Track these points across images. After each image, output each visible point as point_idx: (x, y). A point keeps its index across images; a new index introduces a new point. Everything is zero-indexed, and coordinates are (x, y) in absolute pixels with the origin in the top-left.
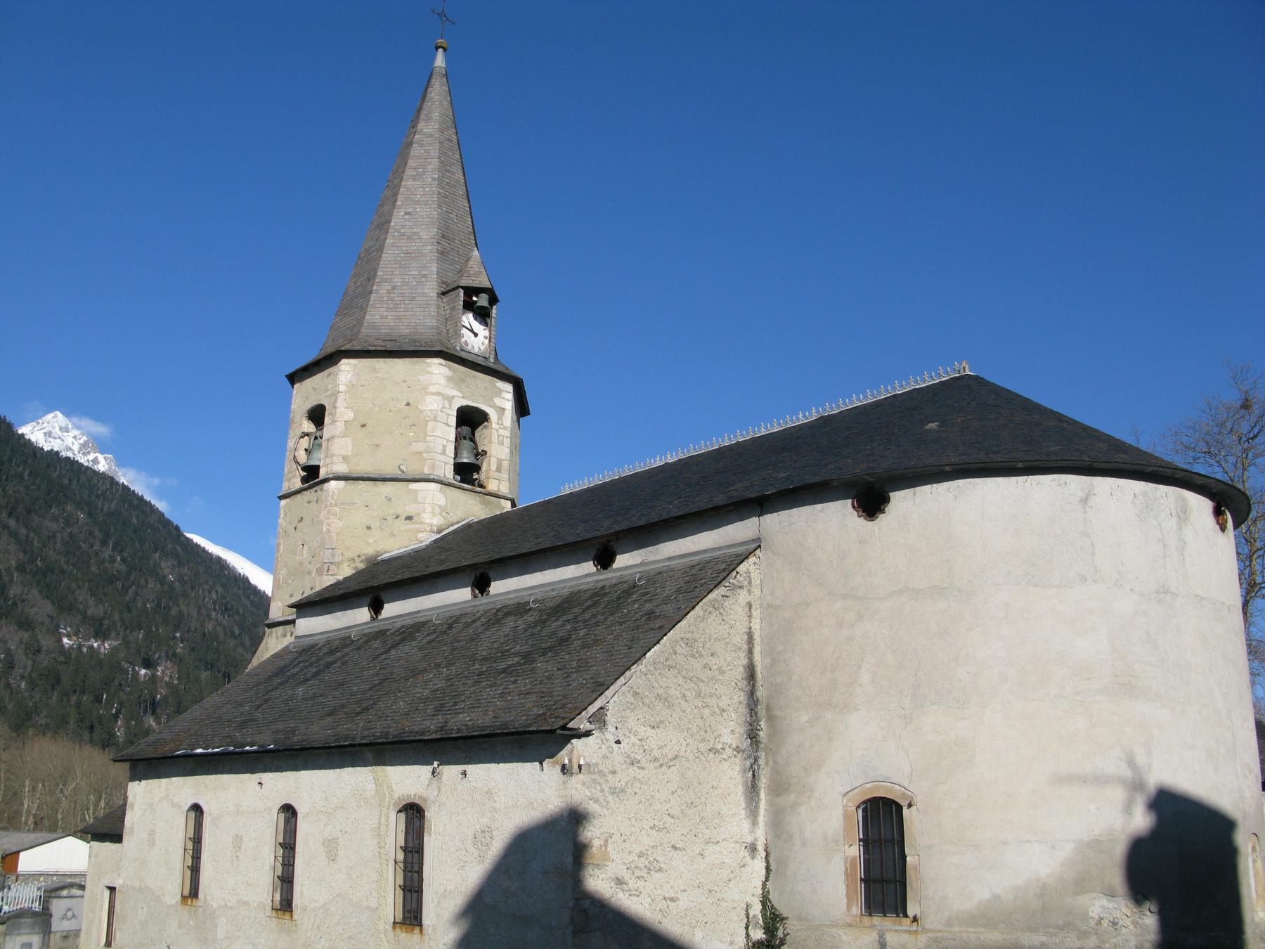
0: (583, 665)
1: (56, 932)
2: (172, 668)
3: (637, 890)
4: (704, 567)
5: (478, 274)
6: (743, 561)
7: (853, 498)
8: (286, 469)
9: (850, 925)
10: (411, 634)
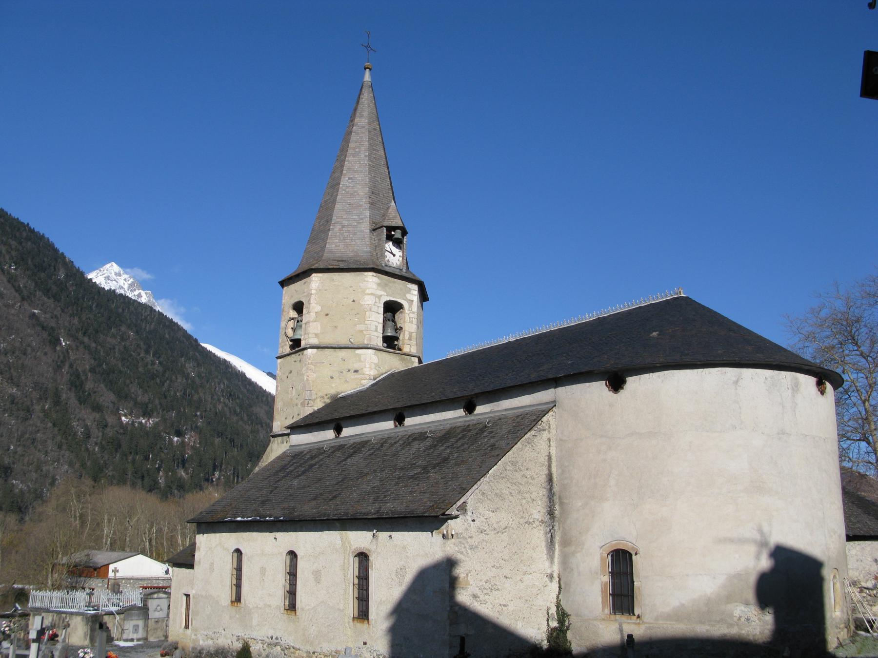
0: (455, 476)
1: (152, 619)
2: (195, 436)
3: (485, 601)
4: (524, 417)
5: (394, 217)
6: (545, 415)
7: (606, 380)
8: (280, 340)
9: (604, 620)
10: (359, 449)
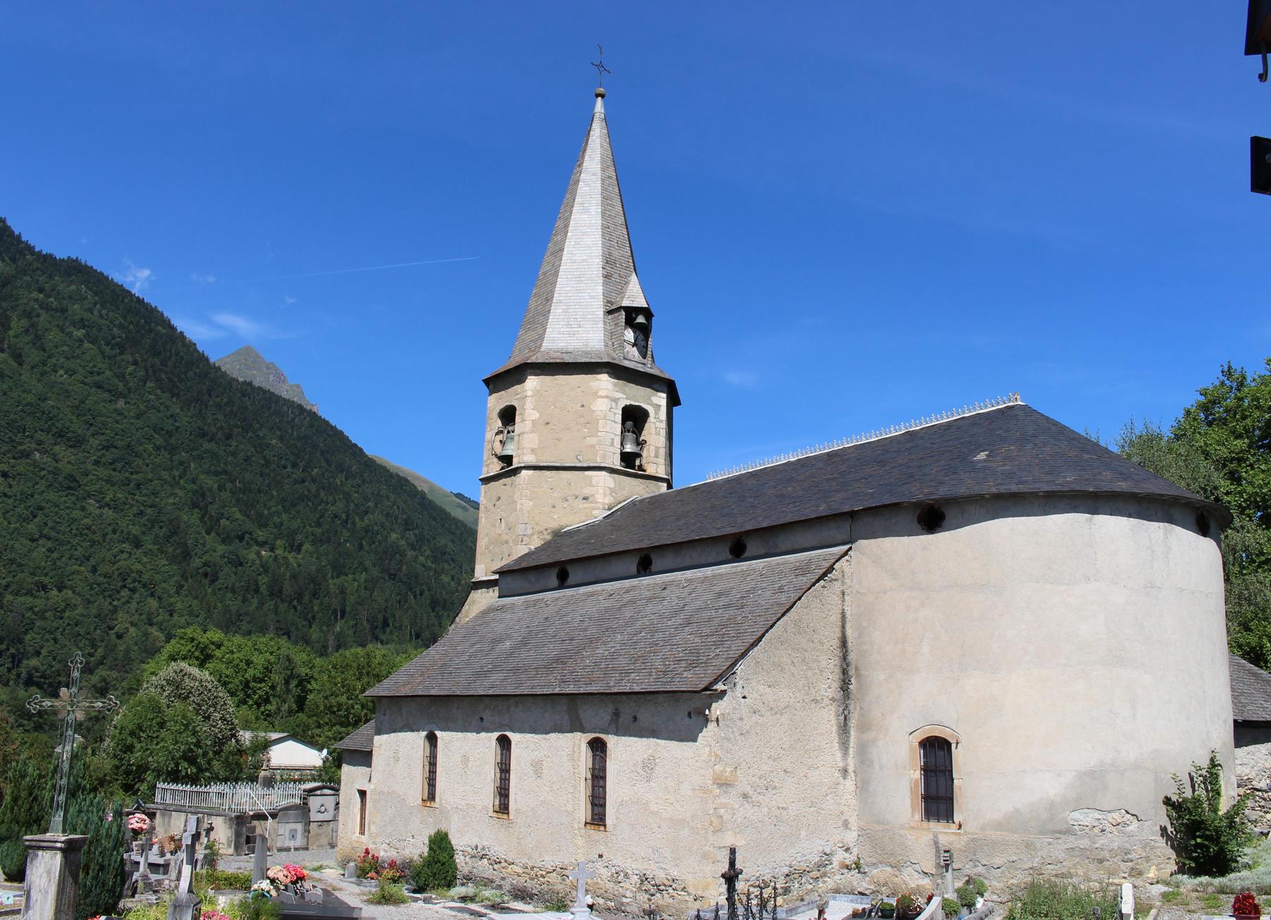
9: (912, 828)
